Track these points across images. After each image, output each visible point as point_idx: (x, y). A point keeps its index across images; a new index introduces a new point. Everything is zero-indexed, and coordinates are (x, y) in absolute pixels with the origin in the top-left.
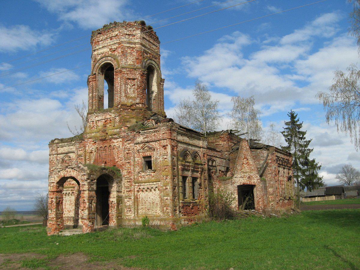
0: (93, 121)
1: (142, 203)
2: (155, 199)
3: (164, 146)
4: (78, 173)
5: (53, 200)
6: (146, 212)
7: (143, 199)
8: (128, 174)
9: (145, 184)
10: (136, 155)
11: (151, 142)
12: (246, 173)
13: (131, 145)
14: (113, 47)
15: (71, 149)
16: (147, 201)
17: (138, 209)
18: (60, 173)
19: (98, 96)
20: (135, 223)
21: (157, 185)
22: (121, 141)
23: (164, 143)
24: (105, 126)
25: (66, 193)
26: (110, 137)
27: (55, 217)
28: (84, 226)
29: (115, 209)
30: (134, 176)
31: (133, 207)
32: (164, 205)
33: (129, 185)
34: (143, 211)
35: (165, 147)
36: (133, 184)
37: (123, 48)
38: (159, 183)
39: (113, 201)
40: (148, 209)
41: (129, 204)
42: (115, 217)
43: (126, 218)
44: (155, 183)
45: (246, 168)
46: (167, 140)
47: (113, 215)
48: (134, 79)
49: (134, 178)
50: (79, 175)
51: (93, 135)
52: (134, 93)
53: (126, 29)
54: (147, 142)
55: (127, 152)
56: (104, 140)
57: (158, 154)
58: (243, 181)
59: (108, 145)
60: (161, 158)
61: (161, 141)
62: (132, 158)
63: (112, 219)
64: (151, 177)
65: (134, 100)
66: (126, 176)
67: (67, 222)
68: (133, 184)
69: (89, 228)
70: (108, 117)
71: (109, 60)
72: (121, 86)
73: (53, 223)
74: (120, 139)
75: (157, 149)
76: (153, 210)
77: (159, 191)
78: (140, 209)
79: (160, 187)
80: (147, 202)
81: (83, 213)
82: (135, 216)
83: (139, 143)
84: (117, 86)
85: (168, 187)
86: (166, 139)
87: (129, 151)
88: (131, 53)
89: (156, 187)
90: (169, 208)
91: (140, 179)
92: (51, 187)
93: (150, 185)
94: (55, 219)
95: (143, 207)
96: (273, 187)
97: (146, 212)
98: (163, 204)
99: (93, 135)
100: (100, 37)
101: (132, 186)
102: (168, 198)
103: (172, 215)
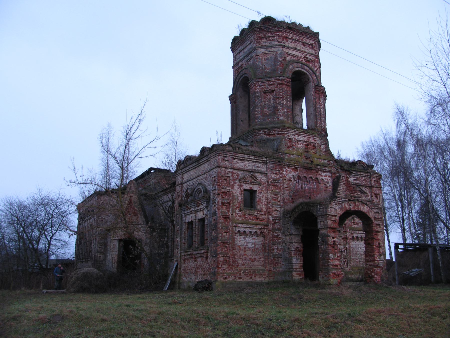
14: (309, 57)
15: (258, 167)
67: (255, 276)
70: (311, 140)
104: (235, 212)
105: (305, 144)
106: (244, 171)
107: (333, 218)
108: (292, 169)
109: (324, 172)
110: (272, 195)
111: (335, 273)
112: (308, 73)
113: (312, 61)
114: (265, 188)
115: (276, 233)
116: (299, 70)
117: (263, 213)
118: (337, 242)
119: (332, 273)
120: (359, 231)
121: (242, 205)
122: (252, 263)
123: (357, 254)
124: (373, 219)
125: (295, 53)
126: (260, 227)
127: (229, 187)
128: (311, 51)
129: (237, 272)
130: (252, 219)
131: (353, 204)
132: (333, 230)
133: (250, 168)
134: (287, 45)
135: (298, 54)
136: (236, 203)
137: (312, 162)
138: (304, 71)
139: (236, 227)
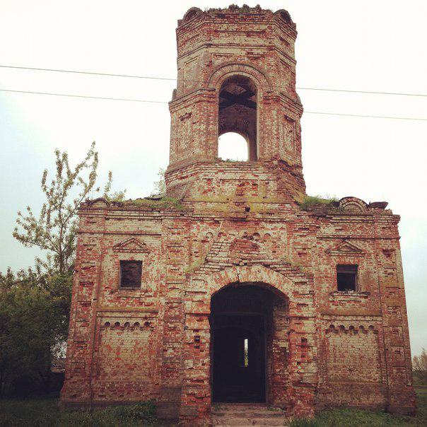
5: (201, 334)
9: (347, 318)
13: (308, 238)
14: (255, 52)
16: (346, 352)
44: (368, 318)
53: (280, 28)
55: (300, 250)
61: (380, 241)
64: (357, 305)
71: (247, 72)
80: (345, 354)
81: (302, 371)
87: (304, 249)
91: (333, 307)
92: (194, 303)
100: (221, 23)
104: (103, 296)
105: (237, 183)
106: (122, 234)
107: (199, 297)
110: (168, 266)
111: (193, 394)
112: (251, 77)
113: (263, 56)
114: (157, 256)
115: (171, 323)
117: (151, 294)
118: (204, 338)
119: (188, 395)
121: (114, 284)
122: (129, 372)
124: (290, 295)
125: (229, 51)
126: (143, 315)
127: (93, 259)
128: (261, 42)
129: (99, 386)
130: (132, 304)
131: (244, 272)
132: (198, 318)
133: (132, 230)
134: (216, 41)
135: (237, 51)
136: (105, 282)
137: (248, 210)
138: (244, 74)
139: (102, 317)
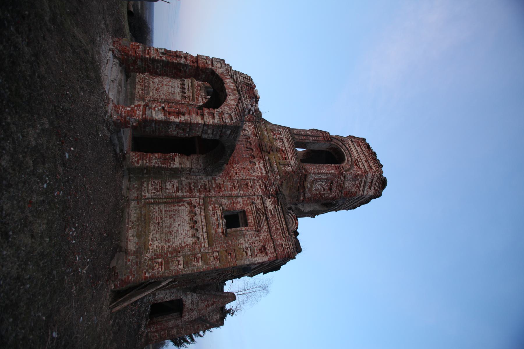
0: (281, 134)
1: (170, 211)
2: (176, 236)
3: (265, 249)
4: (234, 107)
6: (154, 219)
7: (177, 212)
8: (217, 186)
9: (203, 217)
10: (245, 198)
11: (268, 223)
12: (197, 305)
16: (174, 220)
17: (158, 203)
18: (229, 77)
19: (309, 143)
20: (134, 200)
21: (202, 241)
22: (262, 173)
23: (270, 249)
24: (278, 150)
25: (185, 89)
26: (267, 158)
27: (150, 57)
28: (129, 109)
29: (161, 165)
30: (215, 197)
31: (163, 195)
32: (169, 255)
33: (199, 187)
34: (156, 212)
35: (263, 250)
36: (202, 196)
37: (362, 176)
38: (206, 245)
39: (174, 160)
40: (159, 223)
41: (169, 187)
42: (146, 164)
43: (143, 183)
44: (205, 235)
45: (202, 305)
46: (275, 254)
47: (149, 161)
48: (330, 189)
49: (211, 197)
50: (230, 109)
51: (265, 133)
52: (316, 190)
54: (267, 218)
56: (260, 147)
57: (252, 237)
58: (188, 304)
59: (255, 153)
60: (247, 245)
62: (242, 192)
63: (143, 158)
65: (309, 191)
66: (213, 181)
68: (202, 196)
69: (125, 118)
70: (290, 156)
72: (327, 174)
73: (140, 51)
74: (264, 173)
75: (258, 236)
76: (156, 234)
77: (191, 244)
78: (159, 208)
79: (199, 246)
80: (172, 219)
81: (156, 109)
82: (148, 199)
83: (264, 203)
84: (325, 168)
85: (200, 262)
86: (275, 251)
88: (354, 185)
89: (198, 238)
90: (162, 269)
91: (210, 208)
93: (201, 227)
94: (147, 56)
95: (164, 212)
96: (178, 334)
97: (154, 219)
98: (169, 255)
99: (265, 133)
101: (198, 194)
102: (181, 265)
103: (147, 277)
108: (253, 132)
109: (264, 166)
116: (345, 160)
120: (205, 216)
122: (155, 89)
123: (170, 218)
